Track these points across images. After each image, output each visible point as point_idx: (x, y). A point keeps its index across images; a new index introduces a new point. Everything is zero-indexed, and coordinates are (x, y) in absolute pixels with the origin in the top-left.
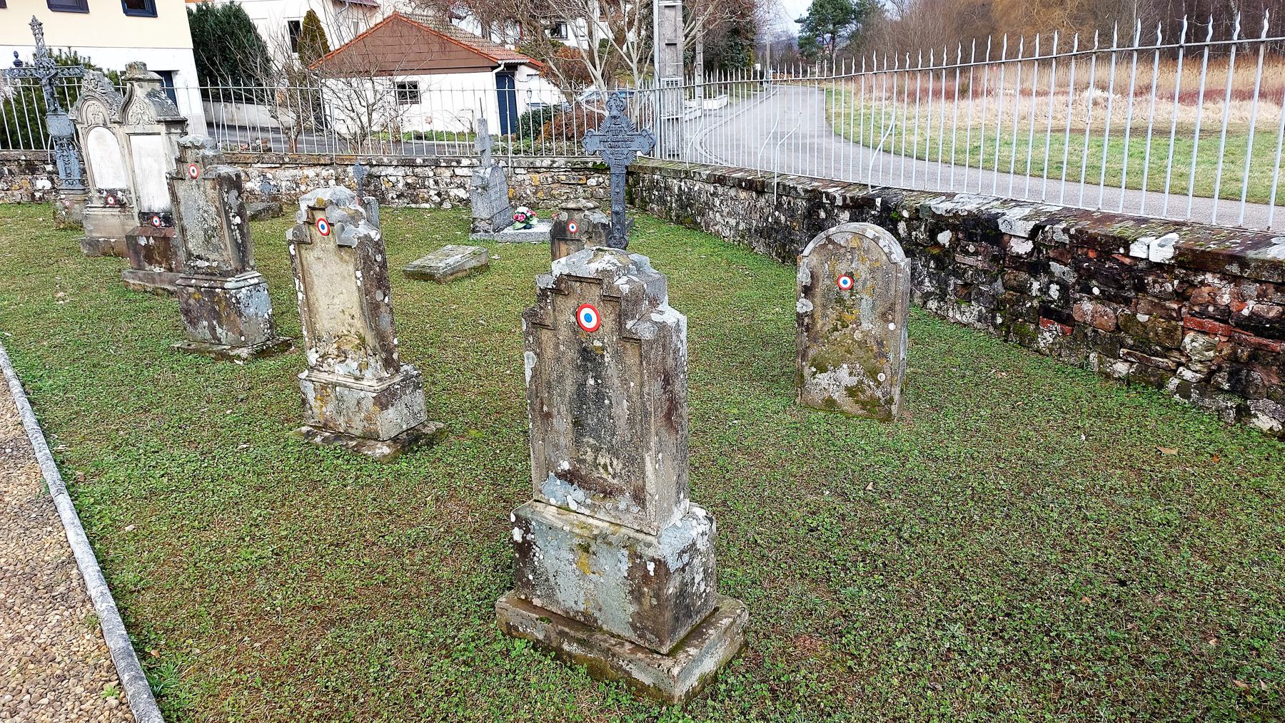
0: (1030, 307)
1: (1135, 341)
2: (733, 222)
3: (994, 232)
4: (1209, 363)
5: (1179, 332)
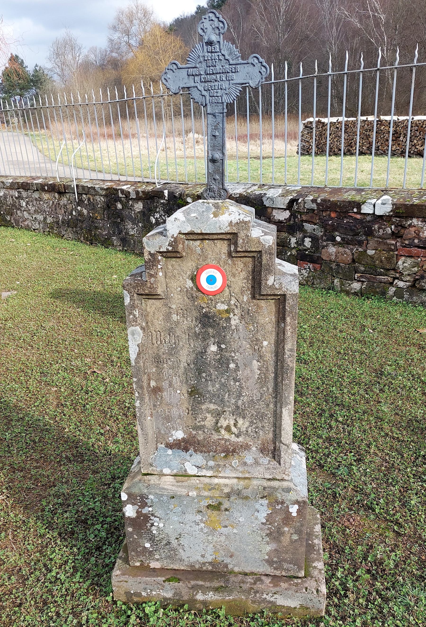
0: (290, 255)
1: (365, 268)
2: (40, 217)
3: (260, 207)
4: (414, 275)
5: (395, 259)
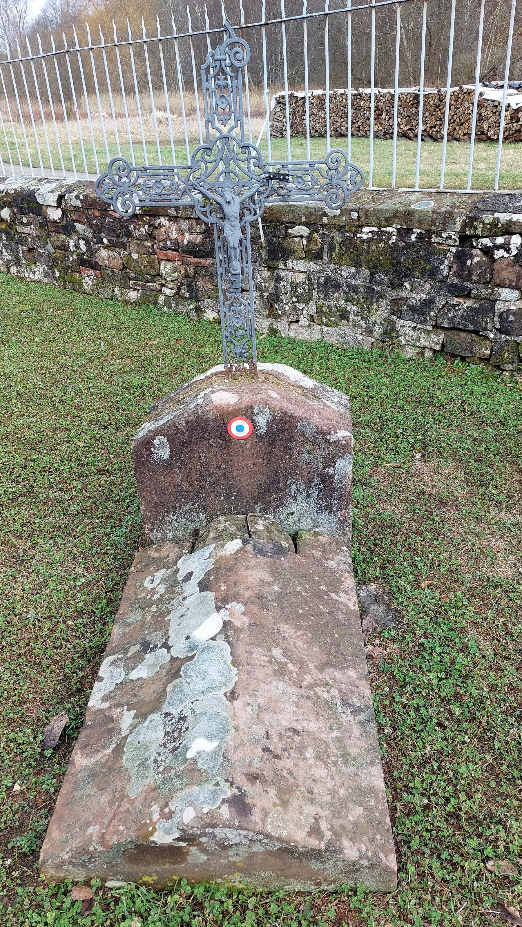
5: (157, 263)
